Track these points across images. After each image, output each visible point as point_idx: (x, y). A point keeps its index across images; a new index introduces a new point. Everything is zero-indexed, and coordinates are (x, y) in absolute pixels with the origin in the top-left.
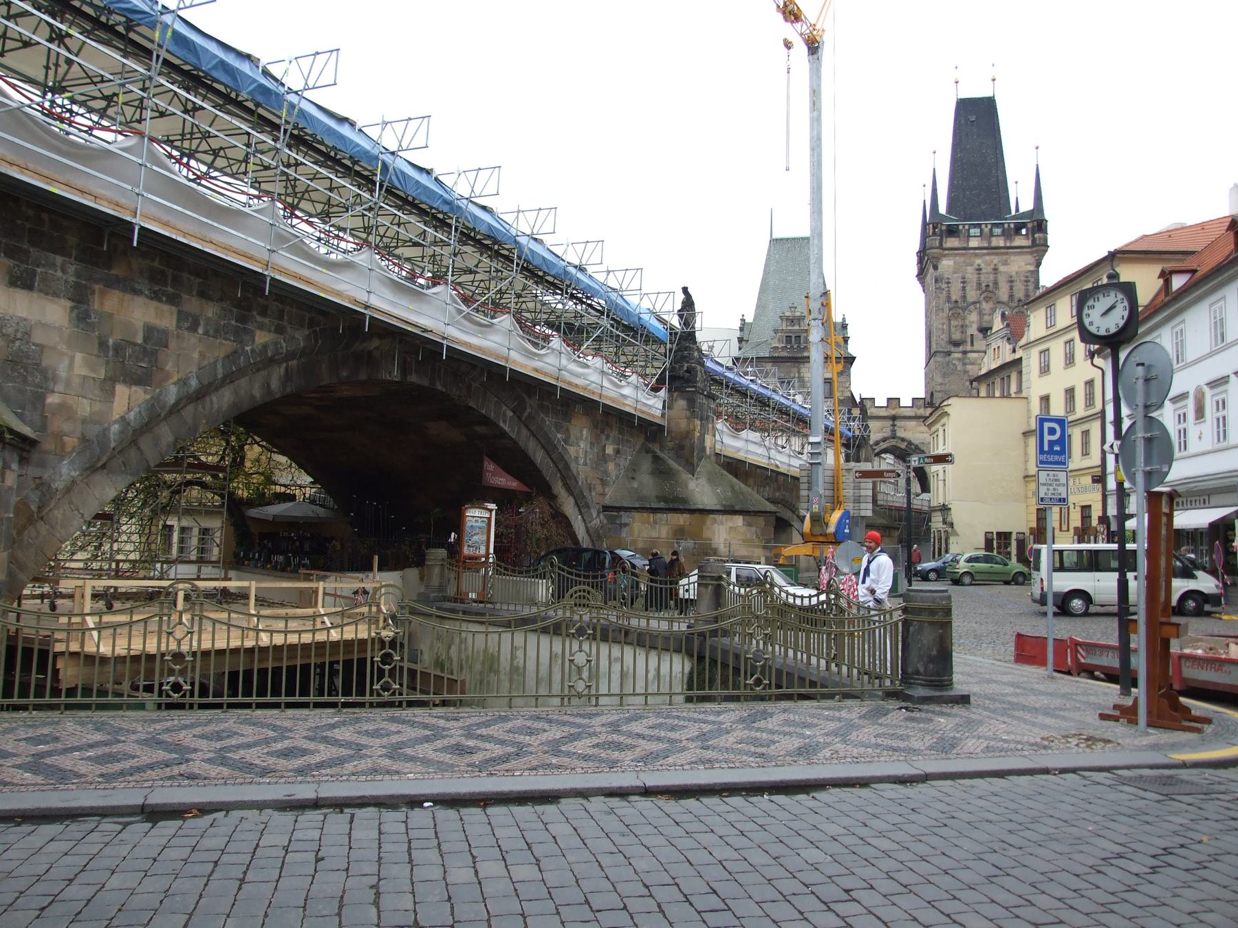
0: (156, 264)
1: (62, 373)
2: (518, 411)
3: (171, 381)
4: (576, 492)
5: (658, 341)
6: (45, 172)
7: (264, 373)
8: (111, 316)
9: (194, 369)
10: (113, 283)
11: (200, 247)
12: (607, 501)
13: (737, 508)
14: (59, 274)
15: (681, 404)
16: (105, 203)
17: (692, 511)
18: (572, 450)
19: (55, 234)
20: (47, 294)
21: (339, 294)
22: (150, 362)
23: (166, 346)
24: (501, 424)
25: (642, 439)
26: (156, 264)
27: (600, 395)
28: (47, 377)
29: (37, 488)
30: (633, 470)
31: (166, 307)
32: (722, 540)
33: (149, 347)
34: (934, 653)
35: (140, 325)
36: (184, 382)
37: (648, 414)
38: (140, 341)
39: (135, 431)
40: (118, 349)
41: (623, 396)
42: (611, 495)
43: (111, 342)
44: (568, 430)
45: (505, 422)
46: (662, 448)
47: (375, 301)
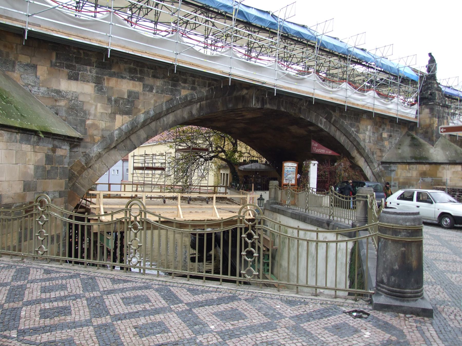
0: (132, 66)
1: (92, 111)
2: (328, 118)
3: (142, 112)
4: (365, 155)
5: (414, 82)
6: (68, 32)
7: (188, 107)
8: (112, 88)
9: (152, 107)
10: (112, 75)
11: (140, 55)
12: (384, 159)
13: (457, 161)
14: (89, 73)
15: (427, 111)
16: (94, 42)
17: (430, 164)
18: (361, 136)
19: (86, 58)
20: (84, 81)
21: (214, 70)
22: (131, 105)
23: (138, 99)
24: (319, 125)
25: (406, 130)
26: (132, 66)
27: (373, 109)
28: (86, 114)
29: (84, 156)
30: (399, 145)
31: (137, 83)
32: (448, 178)
33: (130, 99)
34: (396, 267)
35: (126, 91)
36: (147, 113)
37: (406, 117)
38: (126, 97)
39: (126, 133)
40: (116, 101)
41: (388, 109)
42: (386, 157)
43: (113, 98)
44: (358, 126)
45: (321, 124)
46: (417, 133)
47: (233, 72)
